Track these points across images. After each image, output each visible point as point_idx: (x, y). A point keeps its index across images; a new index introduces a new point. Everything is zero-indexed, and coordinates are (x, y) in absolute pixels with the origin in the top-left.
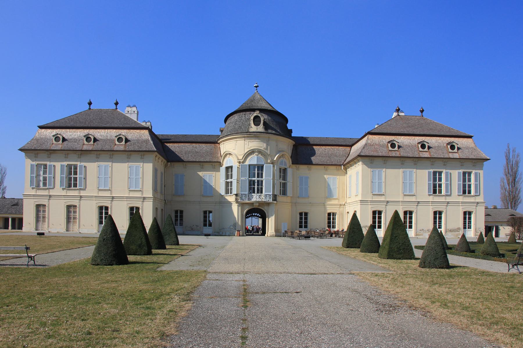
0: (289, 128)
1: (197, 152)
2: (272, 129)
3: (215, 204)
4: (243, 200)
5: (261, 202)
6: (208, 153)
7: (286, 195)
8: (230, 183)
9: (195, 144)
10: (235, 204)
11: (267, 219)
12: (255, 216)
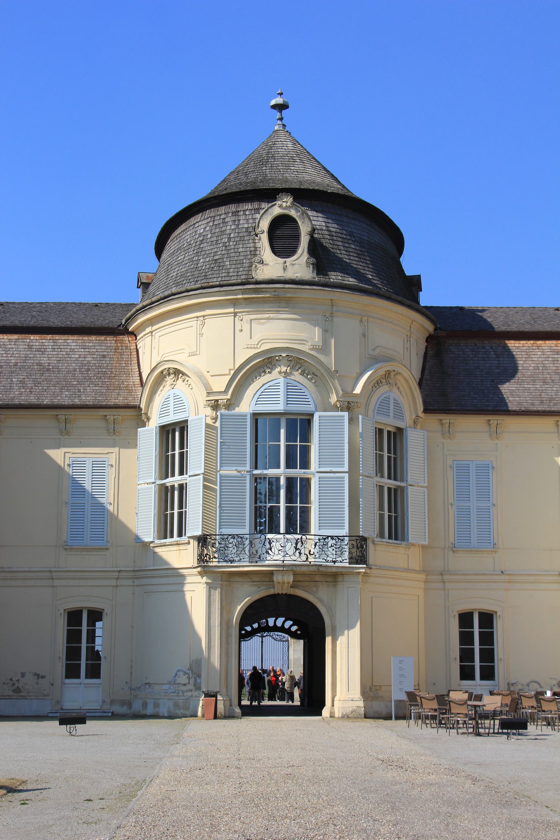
0: (409, 271)
1: (44, 369)
2: (346, 269)
3: (114, 582)
4: (232, 562)
5: (304, 569)
6: (88, 370)
7: (403, 539)
8: (176, 493)
9: (37, 337)
10: (199, 578)
11: (328, 640)
12: (275, 628)
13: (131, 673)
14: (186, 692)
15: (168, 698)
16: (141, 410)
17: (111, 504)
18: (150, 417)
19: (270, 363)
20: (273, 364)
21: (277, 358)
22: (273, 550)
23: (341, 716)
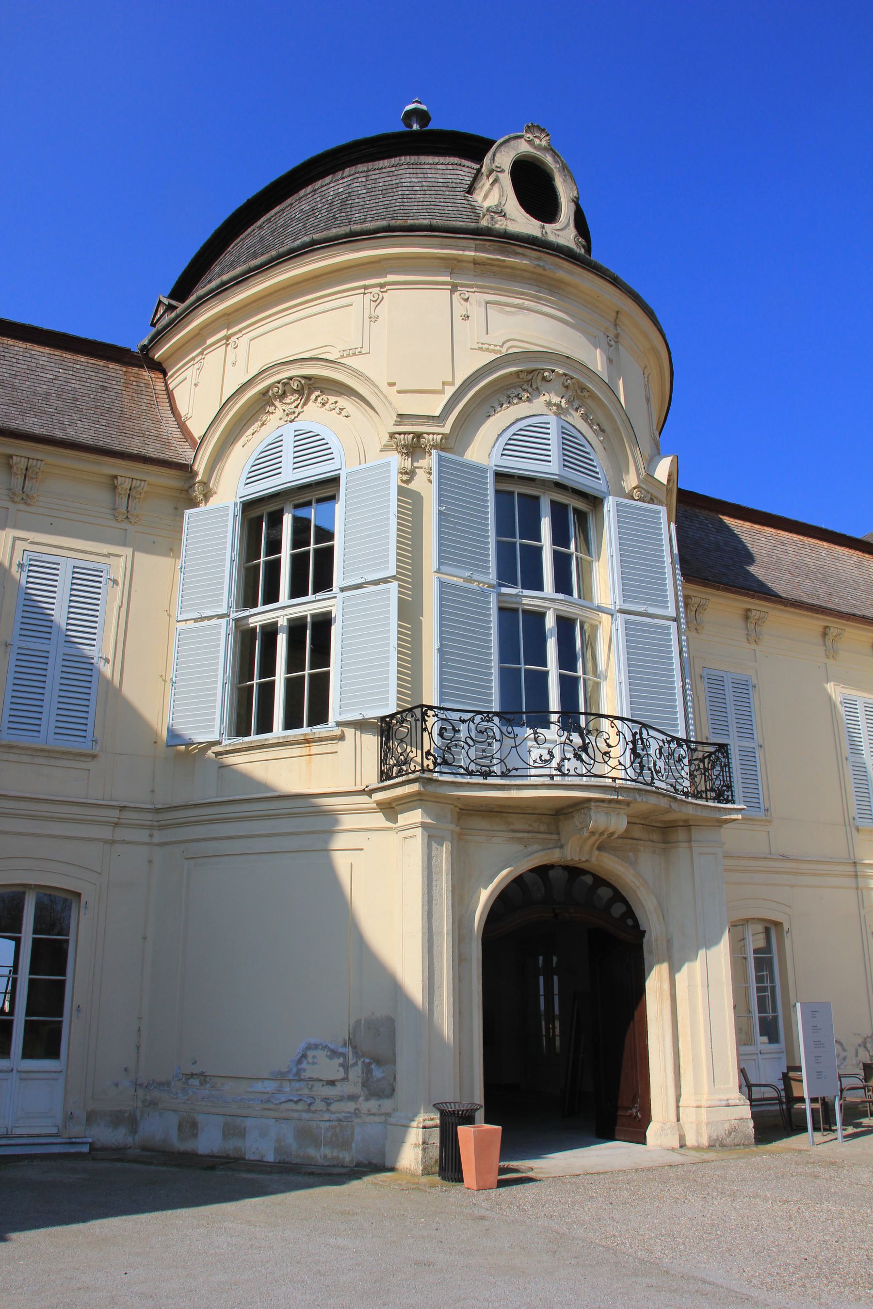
3: (106, 833)
4: (486, 775)
13: (138, 1047)
14: (338, 1100)
15: (277, 1115)
16: (196, 474)
17: (107, 661)
18: (214, 489)
19: (530, 382)
20: (534, 386)
21: (546, 374)
22: (590, 751)
23: (705, 1142)
